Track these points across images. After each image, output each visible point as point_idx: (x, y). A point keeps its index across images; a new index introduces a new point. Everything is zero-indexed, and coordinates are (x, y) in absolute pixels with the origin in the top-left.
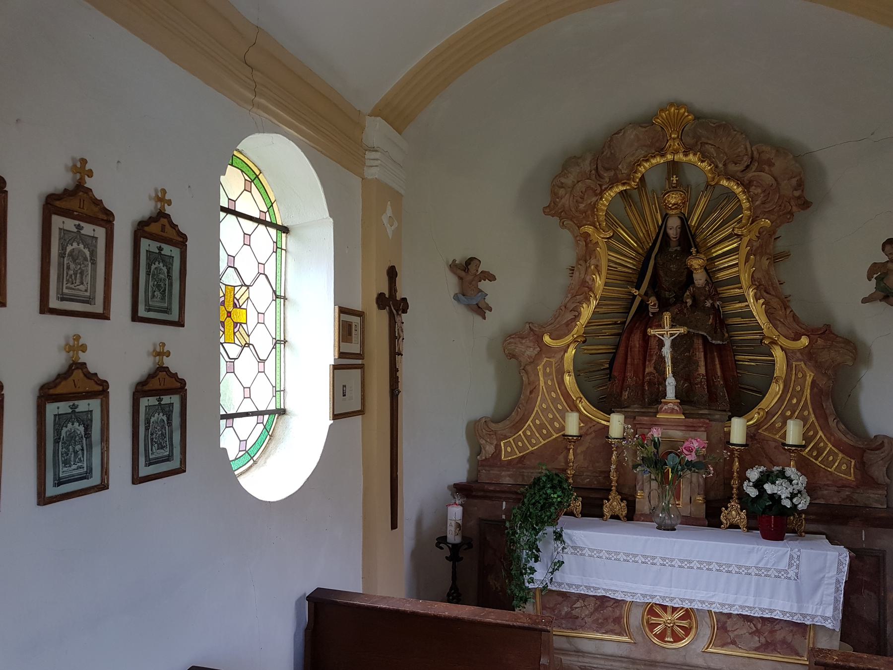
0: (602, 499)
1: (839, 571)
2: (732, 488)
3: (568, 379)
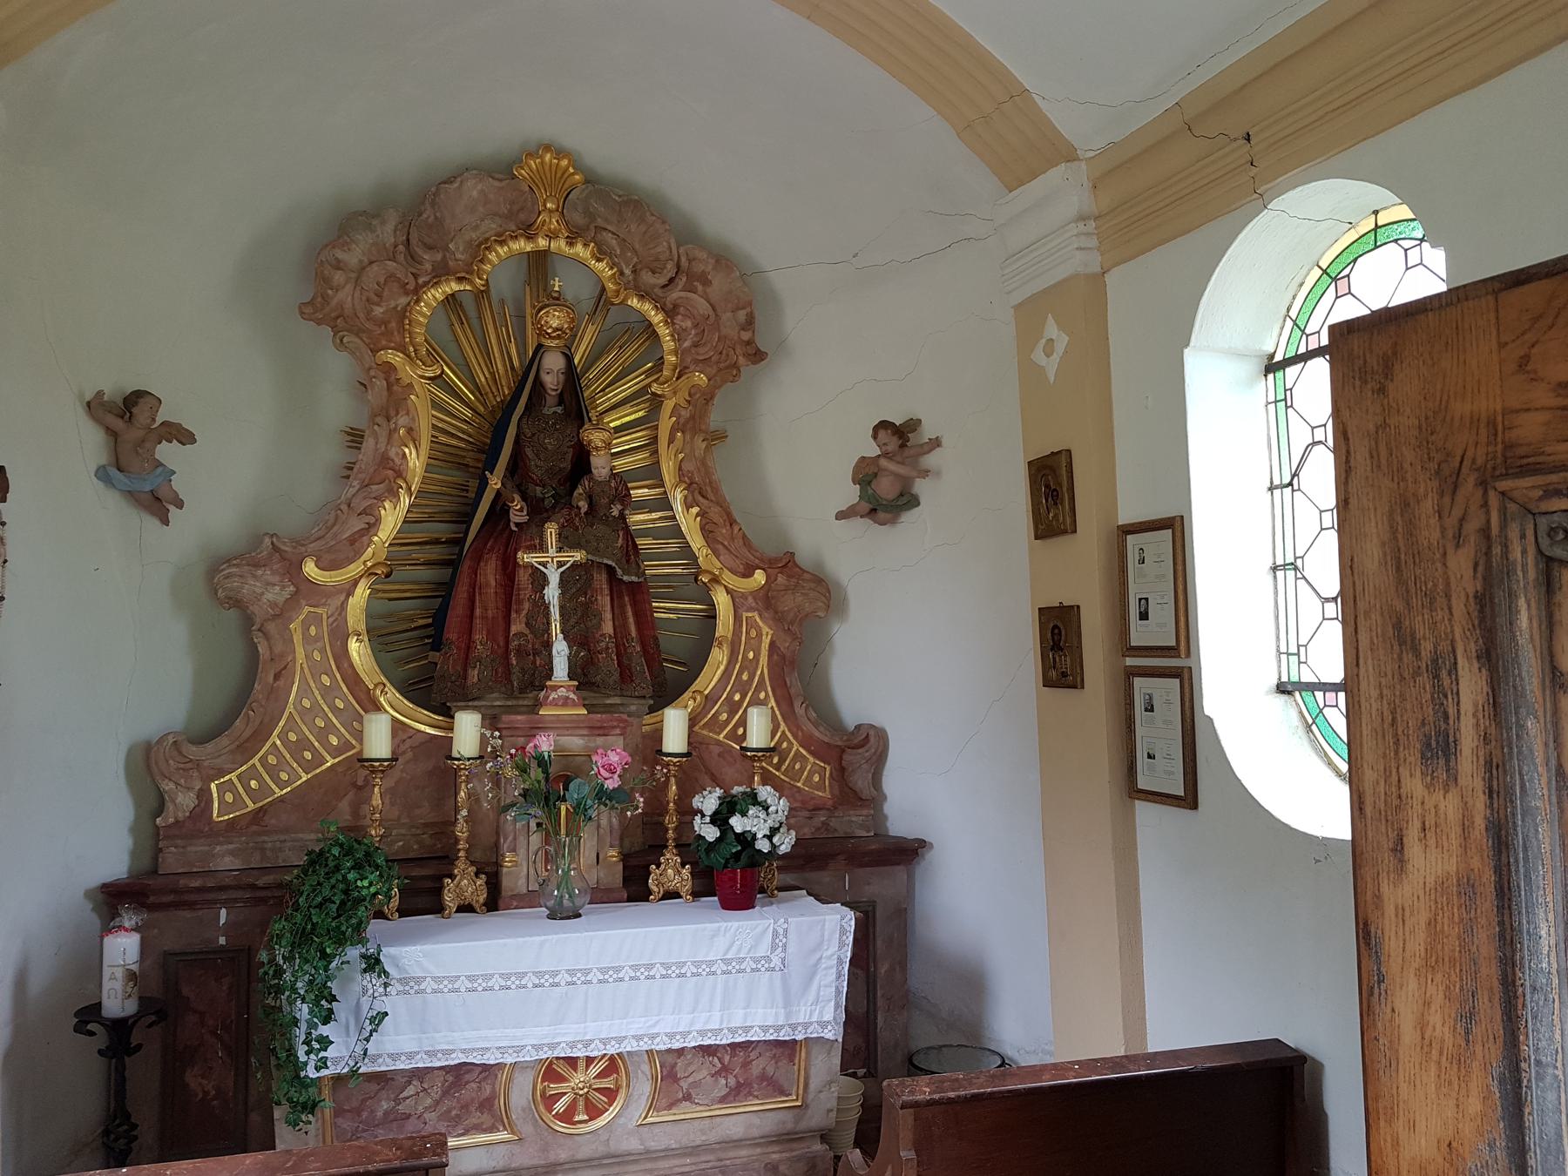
0: (439, 879)
1: (842, 945)
2: (667, 830)
3: (357, 649)
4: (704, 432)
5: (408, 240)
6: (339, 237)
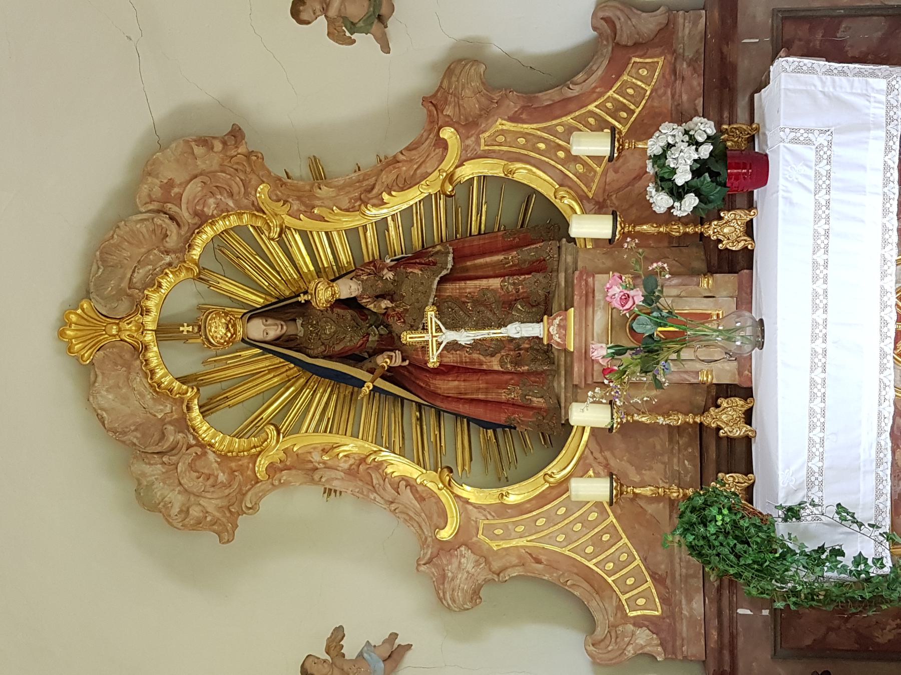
1: (811, 70)
3: (515, 495)
4: (312, 187)
5: (158, 453)
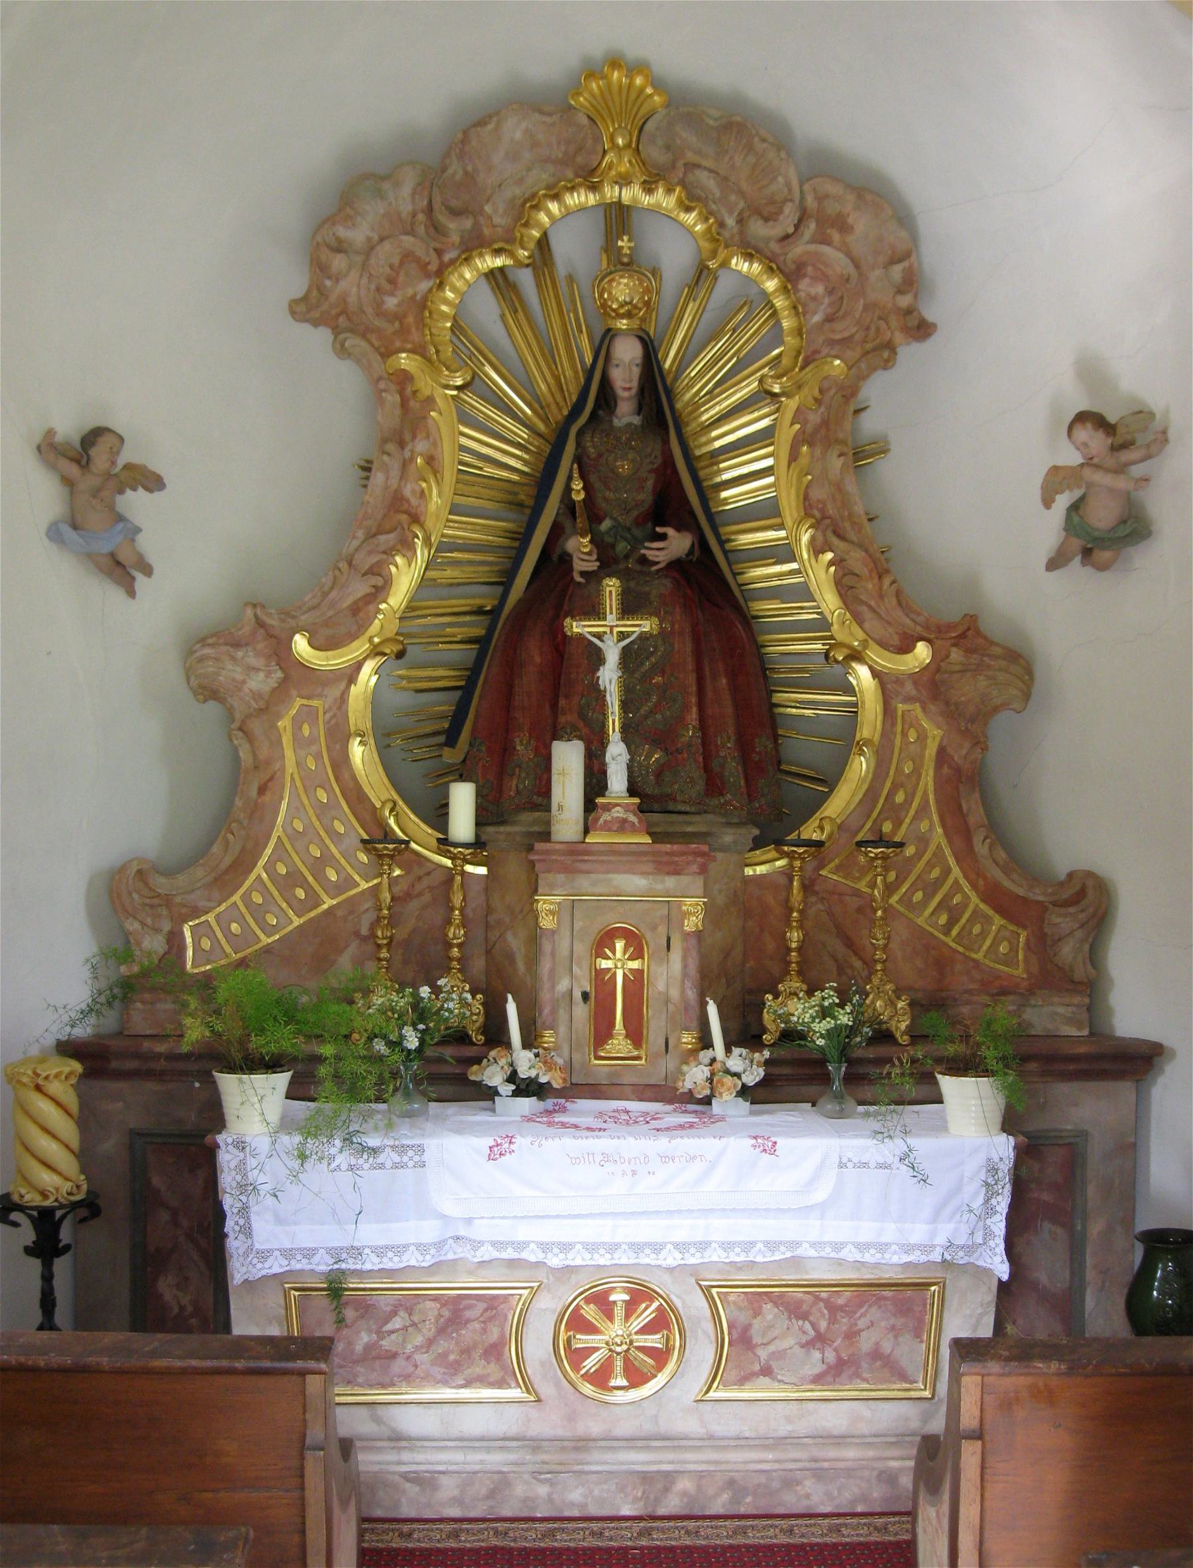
6: (340, 210)
